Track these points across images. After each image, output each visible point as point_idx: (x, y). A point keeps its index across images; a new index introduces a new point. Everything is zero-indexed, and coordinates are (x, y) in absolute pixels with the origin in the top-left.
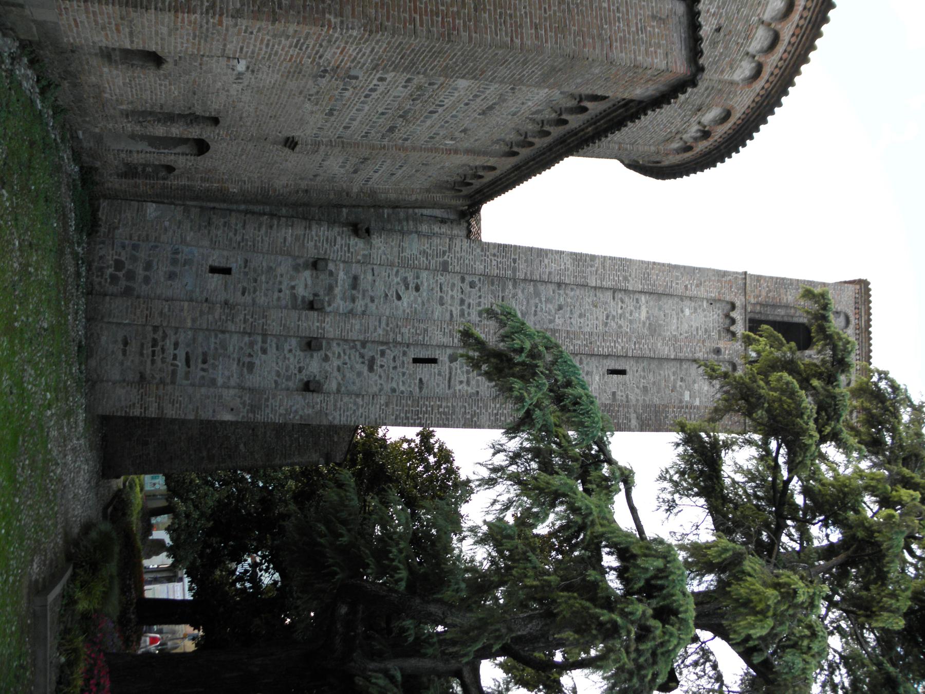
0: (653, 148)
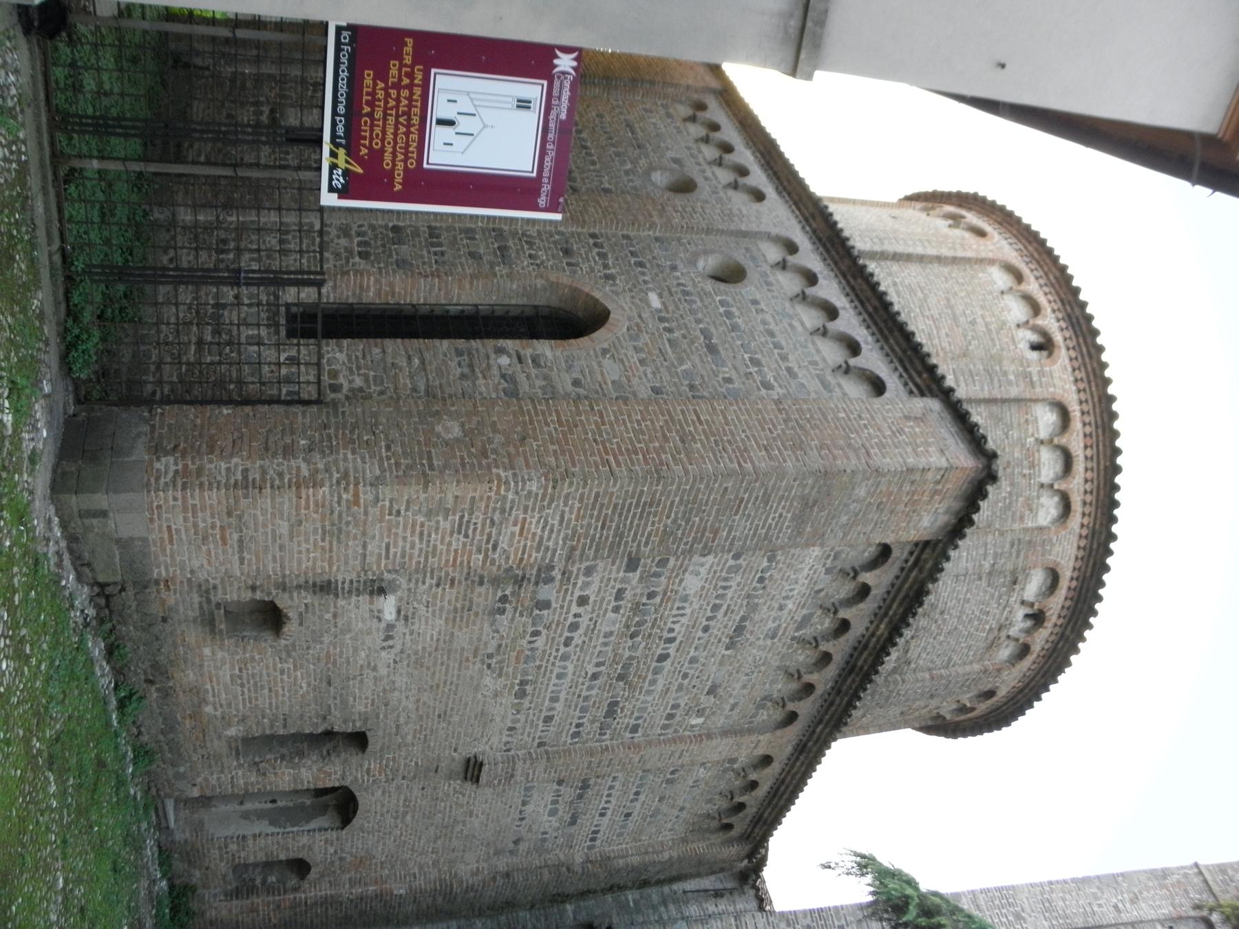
0: (976, 667)
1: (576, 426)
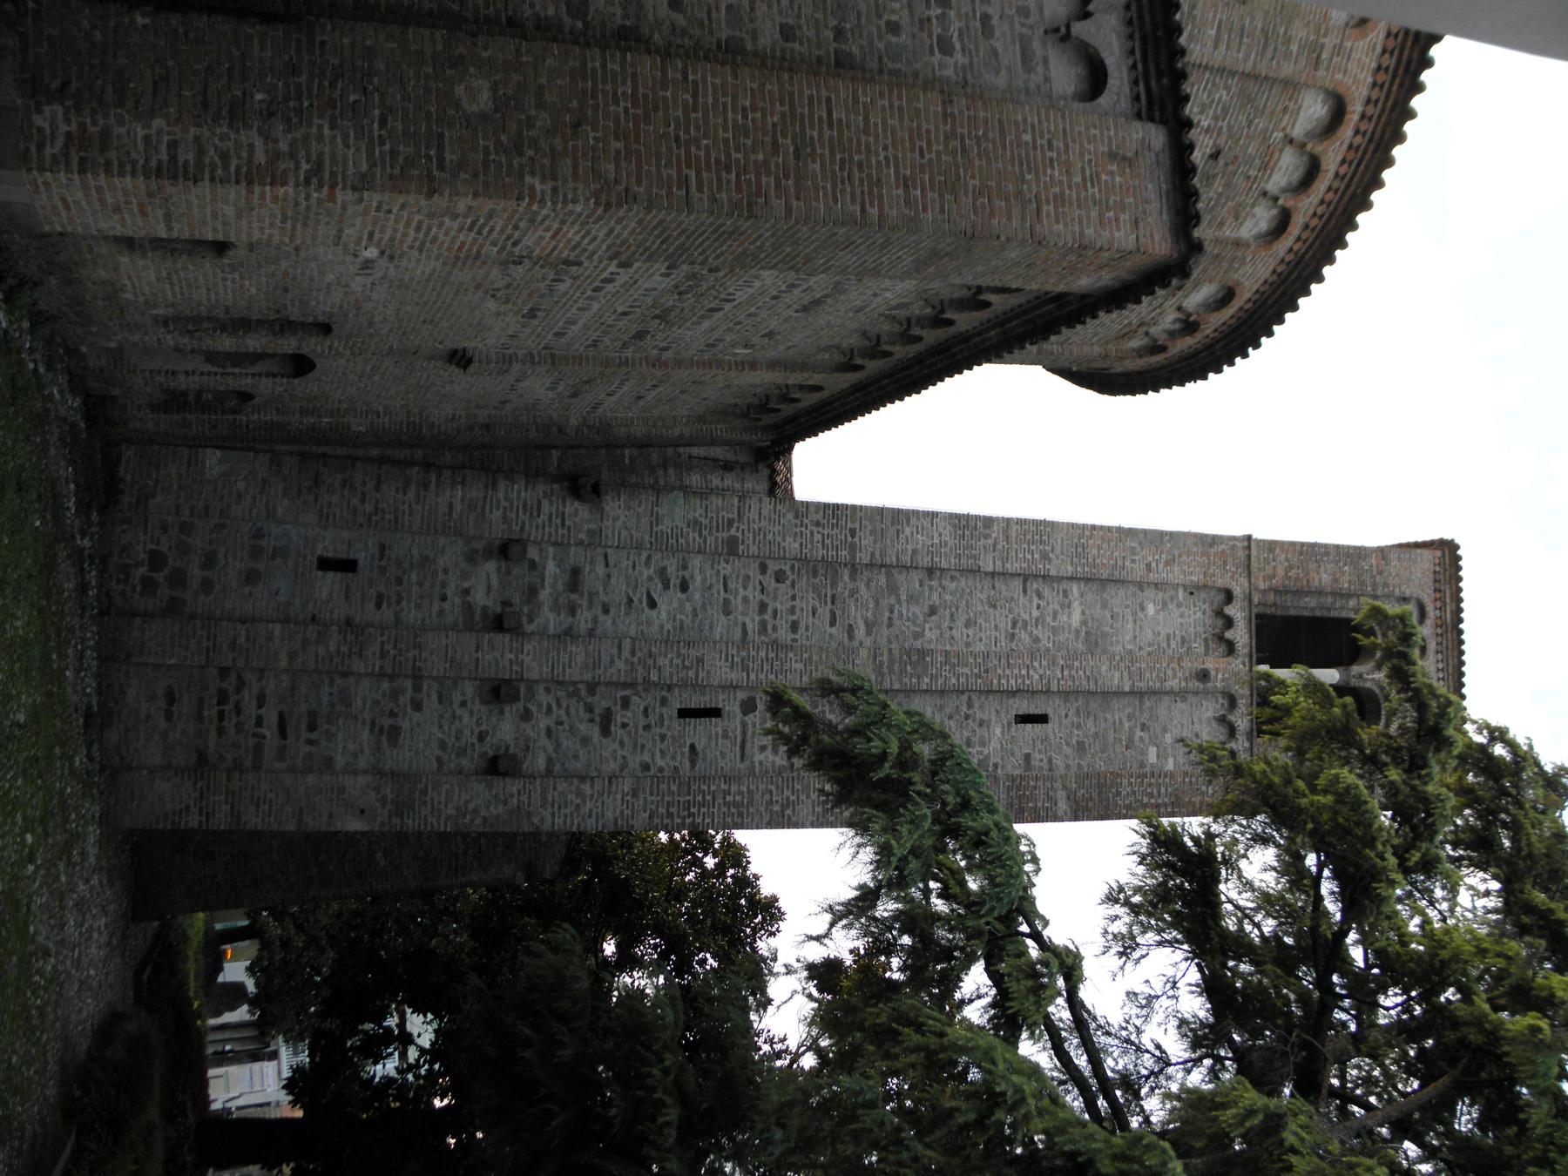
0: (1097, 350)
1: (656, 109)
